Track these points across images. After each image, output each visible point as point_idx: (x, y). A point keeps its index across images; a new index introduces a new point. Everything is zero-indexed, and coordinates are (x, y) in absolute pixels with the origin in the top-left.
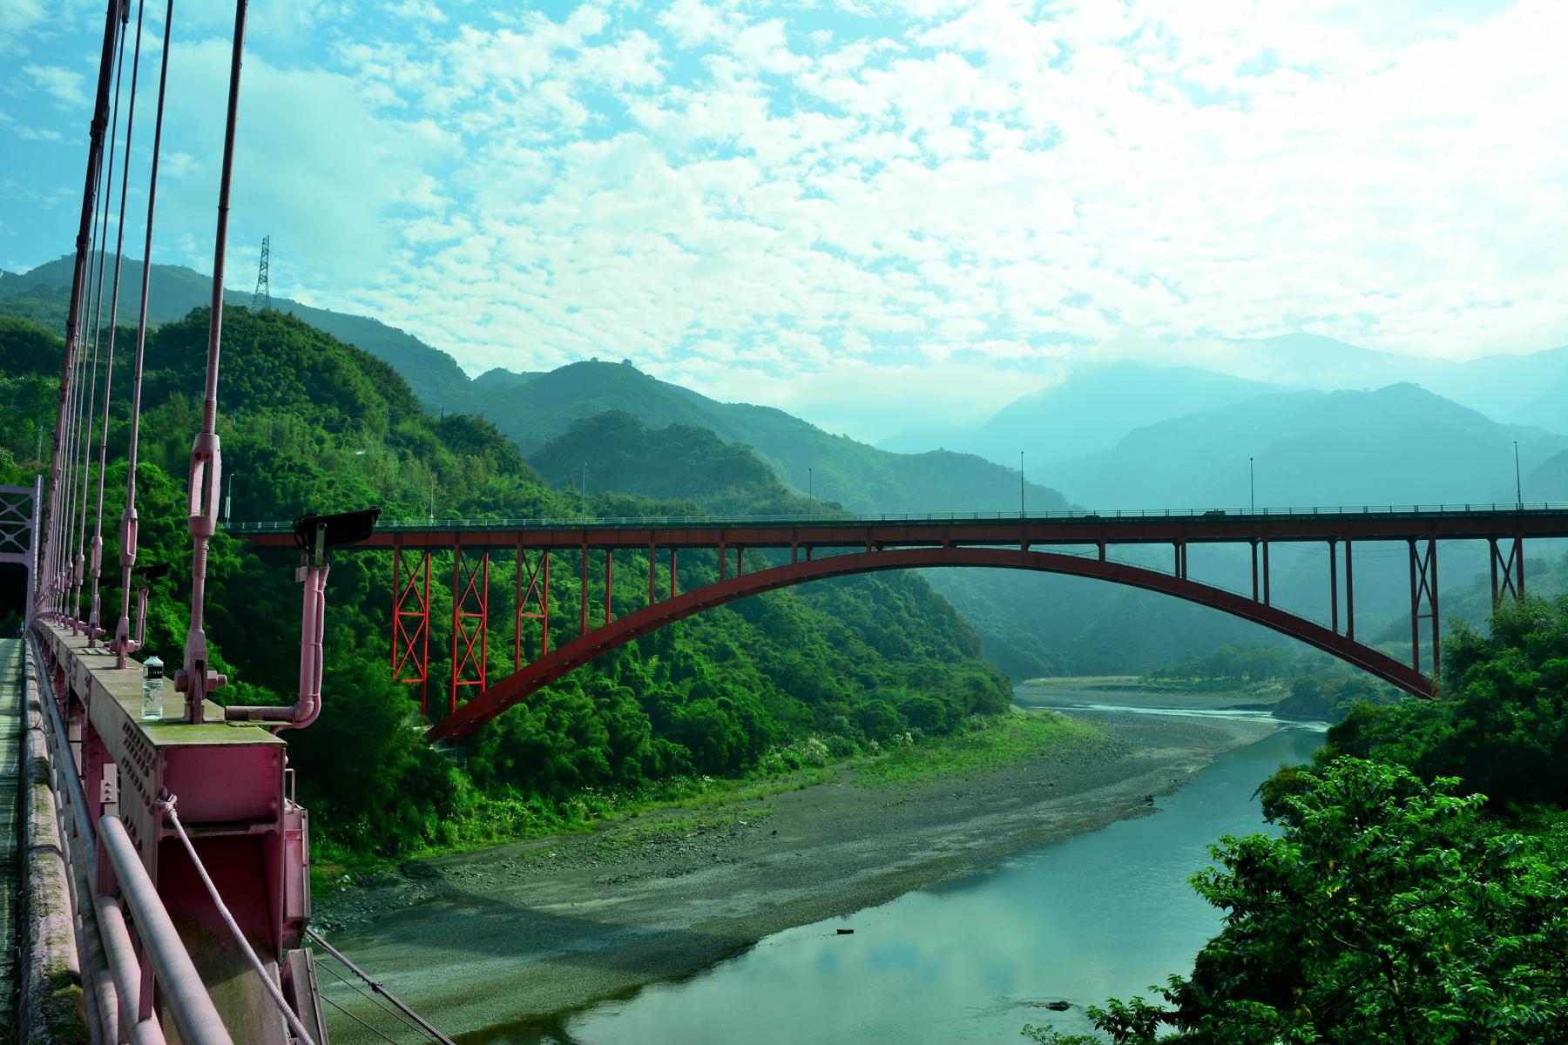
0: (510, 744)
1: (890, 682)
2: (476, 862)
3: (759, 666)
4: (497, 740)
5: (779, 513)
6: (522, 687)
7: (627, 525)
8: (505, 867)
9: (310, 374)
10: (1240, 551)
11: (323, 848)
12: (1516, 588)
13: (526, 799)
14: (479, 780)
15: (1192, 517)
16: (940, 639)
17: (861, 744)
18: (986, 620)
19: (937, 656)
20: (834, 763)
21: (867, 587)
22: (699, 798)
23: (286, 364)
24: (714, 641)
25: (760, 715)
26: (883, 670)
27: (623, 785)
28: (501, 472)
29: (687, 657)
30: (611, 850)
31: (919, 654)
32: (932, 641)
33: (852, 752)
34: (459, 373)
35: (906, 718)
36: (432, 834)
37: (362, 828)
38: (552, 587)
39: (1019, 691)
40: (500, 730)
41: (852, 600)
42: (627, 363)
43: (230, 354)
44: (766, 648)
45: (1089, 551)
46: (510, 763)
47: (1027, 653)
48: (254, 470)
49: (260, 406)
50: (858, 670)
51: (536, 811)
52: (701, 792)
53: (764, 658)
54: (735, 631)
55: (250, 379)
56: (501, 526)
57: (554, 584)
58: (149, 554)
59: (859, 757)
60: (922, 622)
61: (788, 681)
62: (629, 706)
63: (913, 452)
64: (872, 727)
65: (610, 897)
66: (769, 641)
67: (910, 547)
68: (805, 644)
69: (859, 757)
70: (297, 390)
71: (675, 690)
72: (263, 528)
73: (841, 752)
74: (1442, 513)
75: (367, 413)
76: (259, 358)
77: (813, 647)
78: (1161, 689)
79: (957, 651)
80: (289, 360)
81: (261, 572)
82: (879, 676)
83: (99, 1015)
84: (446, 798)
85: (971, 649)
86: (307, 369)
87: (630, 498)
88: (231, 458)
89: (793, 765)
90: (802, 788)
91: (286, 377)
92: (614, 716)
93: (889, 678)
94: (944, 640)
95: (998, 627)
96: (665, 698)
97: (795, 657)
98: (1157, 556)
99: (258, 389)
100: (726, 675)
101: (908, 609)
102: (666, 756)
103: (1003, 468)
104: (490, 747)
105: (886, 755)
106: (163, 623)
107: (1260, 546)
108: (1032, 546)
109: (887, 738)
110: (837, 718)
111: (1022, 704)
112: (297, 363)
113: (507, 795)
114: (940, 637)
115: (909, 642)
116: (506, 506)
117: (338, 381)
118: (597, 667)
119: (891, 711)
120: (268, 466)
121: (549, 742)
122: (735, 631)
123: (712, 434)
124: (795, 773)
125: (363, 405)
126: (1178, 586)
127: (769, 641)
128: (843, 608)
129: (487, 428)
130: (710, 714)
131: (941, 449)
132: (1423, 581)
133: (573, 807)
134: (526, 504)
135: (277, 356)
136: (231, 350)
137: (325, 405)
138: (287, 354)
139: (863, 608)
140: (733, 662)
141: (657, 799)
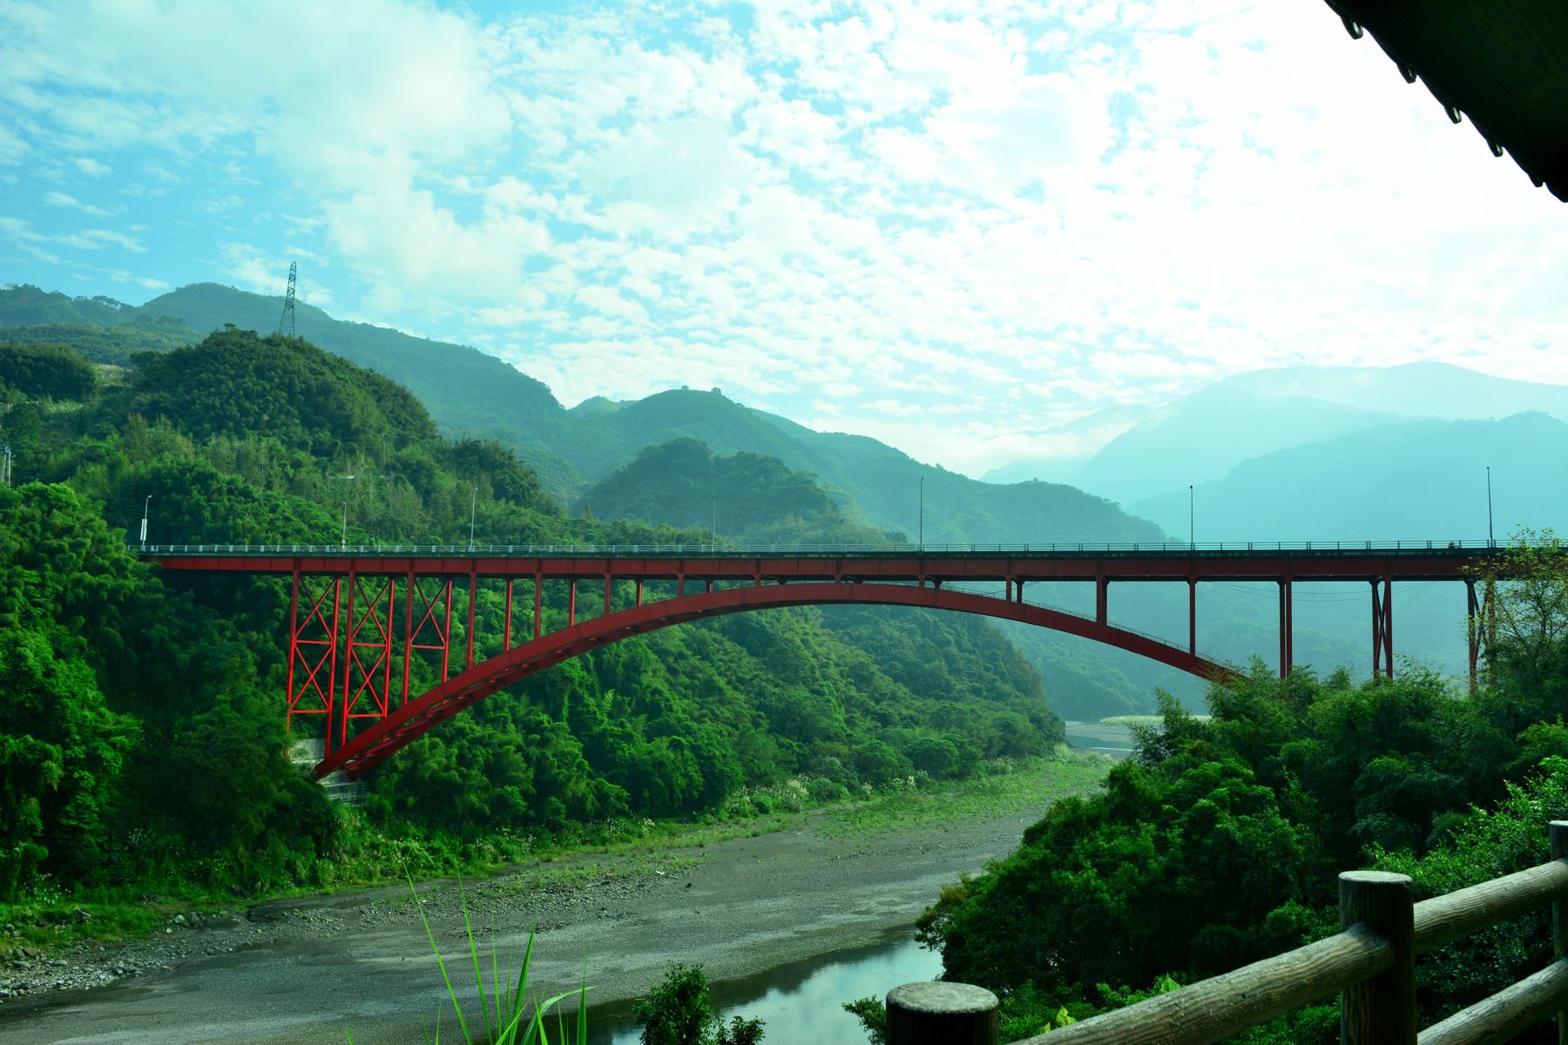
0: (410, 780)
1: (911, 721)
2: (334, 906)
3: (754, 702)
4: (396, 777)
5: (830, 542)
6: (432, 717)
7: (640, 554)
8: (362, 912)
9: (302, 398)
11: (170, 885)
13: (427, 839)
14: (375, 817)
15: (1109, 552)
17: (851, 788)
18: (1071, 655)
19: (984, 693)
20: (814, 807)
21: (915, 620)
22: (636, 841)
23: (278, 387)
24: (700, 675)
25: (724, 756)
26: (908, 708)
27: (514, 826)
28: (497, 497)
29: (656, 691)
30: (493, 898)
31: (962, 691)
32: (981, 677)
33: (839, 797)
34: (552, 401)
35: (910, 762)
36: (304, 873)
37: (219, 867)
38: (514, 616)
40: (401, 765)
42: (716, 391)
43: (224, 377)
44: (764, 684)
45: (995, 589)
46: (411, 801)
47: (1112, 690)
48: (189, 493)
49: (246, 430)
50: (878, 708)
51: (433, 851)
52: (640, 836)
53: (761, 694)
54: (733, 665)
55: (238, 404)
56: (487, 553)
57: (517, 614)
58: (32, 576)
59: (847, 804)
60: (973, 657)
61: (787, 722)
63: (1006, 483)
64: (870, 770)
65: (451, 952)
66: (770, 676)
67: (803, 582)
68: (817, 680)
69: (847, 804)
70: (288, 414)
72: (174, 552)
73: (823, 796)
74: (1399, 550)
75: (362, 436)
76: (249, 382)
77: (824, 683)
79: (1007, 688)
80: (282, 383)
81: (160, 596)
82: (900, 714)
83: (421, 987)
84: (330, 833)
85: (1030, 687)
86: (301, 393)
87: (647, 526)
88: (169, 481)
89: (762, 809)
90: (755, 835)
91: (277, 401)
92: (543, 755)
93: (911, 718)
94: (994, 677)
96: (612, 736)
97: (800, 693)
99: (244, 412)
100: (705, 711)
101: (959, 644)
102: (602, 797)
103: (1098, 500)
104: (389, 782)
105: (878, 800)
106: (22, 646)
107: (1381, 586)
109: (885, 781)
110: (828, 759)
112: (289, 388)
113: (406, 835)
115: (952, 679)
116: (494, 533)
117: (333, 405)
119: (890, 752)
120: (206, 491)
121: (459, 779)
122: (733, 665)
124: (762, 817)
125: (357, 429)
127: (770, 676)
128: (886, 642)
129: (503, 454)
130: (657, 754)
131: (1035, 479)
133: (480, 850)
134: (513, 532)
135: (270, 380)
136: (226, 374)
137: (316, 429)
138: (280, 378)
139: (907, 641)
141: (584, 843)
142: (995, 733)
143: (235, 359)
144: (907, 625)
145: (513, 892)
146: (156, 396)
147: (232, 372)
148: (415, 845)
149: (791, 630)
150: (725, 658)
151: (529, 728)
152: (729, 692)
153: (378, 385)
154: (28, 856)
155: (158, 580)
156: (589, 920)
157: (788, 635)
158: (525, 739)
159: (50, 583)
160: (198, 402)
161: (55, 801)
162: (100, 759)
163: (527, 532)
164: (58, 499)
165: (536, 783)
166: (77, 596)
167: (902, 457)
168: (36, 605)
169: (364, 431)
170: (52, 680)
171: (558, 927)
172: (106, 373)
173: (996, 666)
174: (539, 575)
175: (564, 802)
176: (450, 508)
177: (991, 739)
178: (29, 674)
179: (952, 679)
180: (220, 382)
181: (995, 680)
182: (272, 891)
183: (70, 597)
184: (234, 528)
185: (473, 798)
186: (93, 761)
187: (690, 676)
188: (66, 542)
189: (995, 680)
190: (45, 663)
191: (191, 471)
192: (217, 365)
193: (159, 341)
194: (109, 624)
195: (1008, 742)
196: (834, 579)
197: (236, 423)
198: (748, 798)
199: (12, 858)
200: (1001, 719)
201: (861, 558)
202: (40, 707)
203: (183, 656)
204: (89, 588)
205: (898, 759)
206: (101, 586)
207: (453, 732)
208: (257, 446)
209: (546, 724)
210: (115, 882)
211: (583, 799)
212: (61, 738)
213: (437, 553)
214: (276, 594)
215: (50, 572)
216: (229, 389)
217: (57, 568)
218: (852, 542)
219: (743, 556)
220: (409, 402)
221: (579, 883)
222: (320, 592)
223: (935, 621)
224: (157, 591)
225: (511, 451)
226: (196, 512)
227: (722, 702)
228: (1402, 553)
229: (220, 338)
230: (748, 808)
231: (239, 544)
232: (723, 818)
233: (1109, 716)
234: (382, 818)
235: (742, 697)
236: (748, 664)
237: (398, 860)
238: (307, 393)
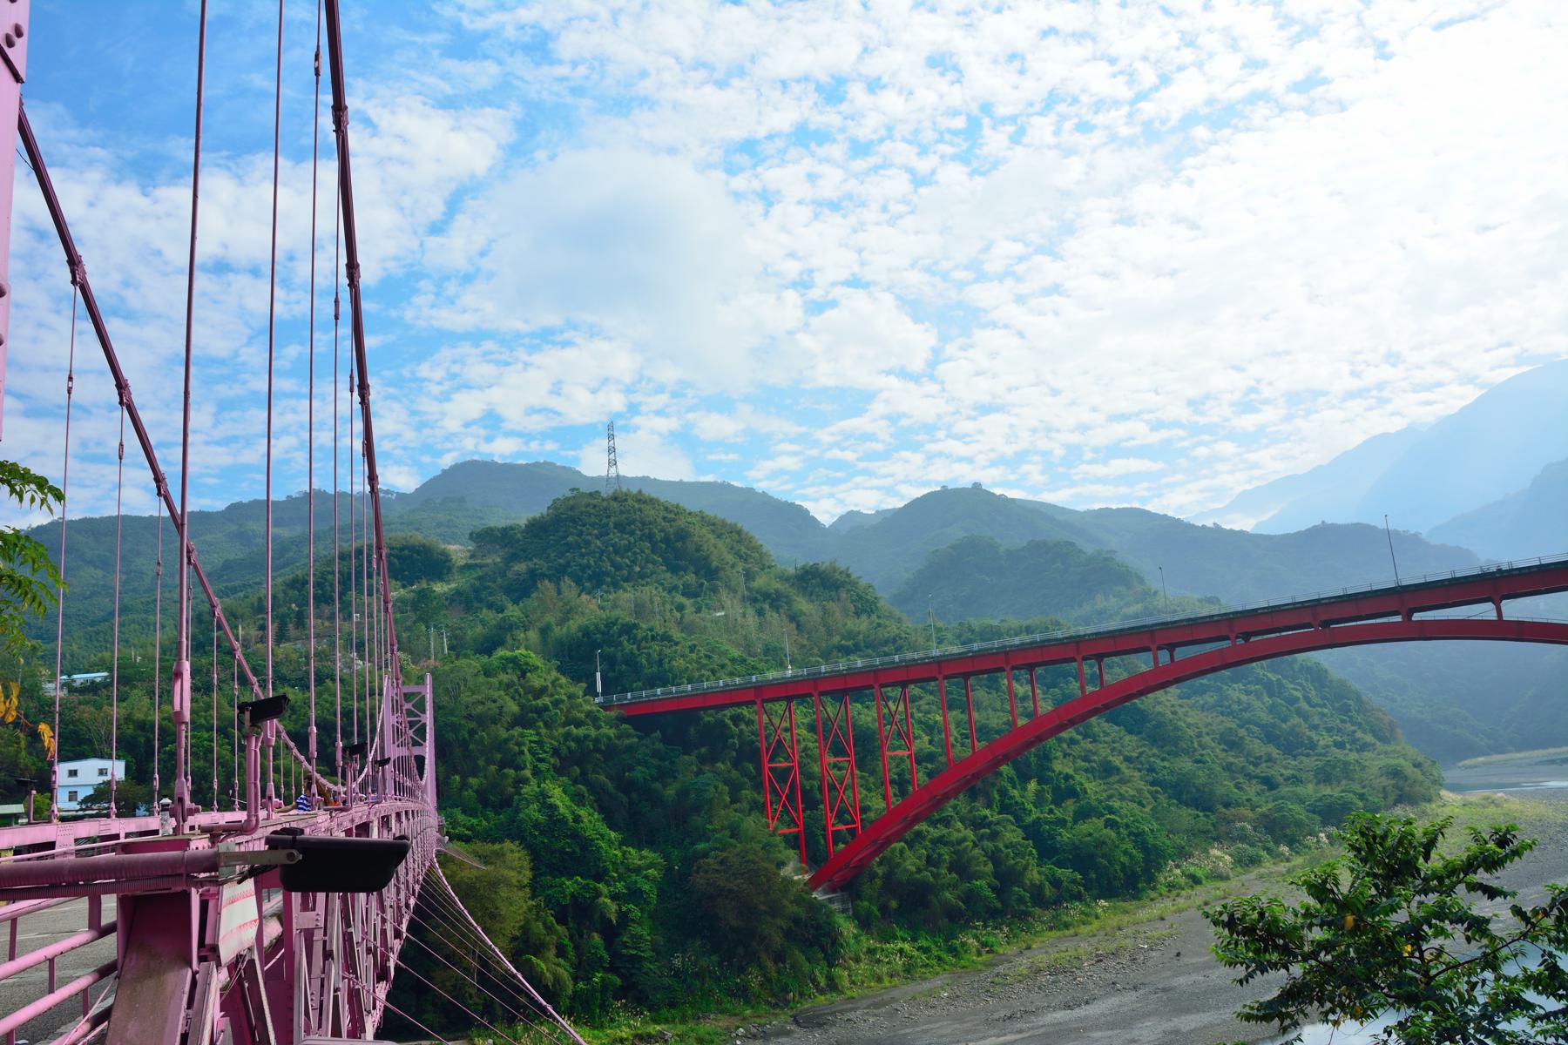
3: (1148, 778)
4: (878, 882)
6: (899, 822)
8: (897, 1010)
9: (664, 546)
13: (914, 940)
14: (864, 923)
17: (1268, 850)
19: (1348, 746)
22: (1096, 924)
23: (640, 539)
24: (1095, 758)
25: (1152, 831)
29: (1067, 777)
30: (1005, 985)
31: (1328, 746)
32: (1339, 730)
33: (1260, 861)
35: (1318, 818)
36: (823, 983)
37: (754, 980)
40: (880, 871)
41: (1244, 698)
43: (589, 537)
44: (1152, 759)
45: (1484, 611)
48: (620, 644)
50: (1258, 771)
51: (925, 950)
52: (1097, 917)
53: (1151, 770)
54: (1117, 745)
55: (610, 560)
60: (1326, 711)
61: (1183, 792)
62: (1013, 835)
65: (1005, 1035)
70: (654, 562)
75: (722, 574)
76: (615, 538)
77: (1204, 752)
79: (1369, 738)
80: (643, 535)
82: (1282, 775)
86: (661, 541)
87: (995, 623)
89: (1195, 880)
91: (643, 552)
92: (996, 847)
93: (1294, 777)
94: (1353, 728)
97: (1186, 764)
99: (618, 567)
102: (1056, 883)
104: (871, 889)
109: (1298, 841)
110: (1238, 825)
112: (650, 537)
113: (895, 937)
114: (1348, 725)
115: (1313, 734)
116: (867, 647)
119: (1299, 811)
120: (633, 640)
121: (931, 879)
122: (1117, 745)
124: (1198, 888)
127: (1155, 751)
128: (1235, 707)
129: (841, 573)
131: (1323, 522)
133: (963, 944)
134: (886, 643)
135: (632, 533)
137: (682, 573)
138: (641, 530)
141: (1051, 929)
142: (1385, 781)
143: (593, 519)
144: (1252, 688)
145: (1020, 978)
146: (531, 565)
147: (596, 532)
148: (906, 946)
149: (1159, 703)
150: (1106, 739)
151: (977, 824)
153: (714, 524)
154: (605, 985)
155: (627, 726)
156: (1108, 995)
157: (1159, 709)
158: (976, 835)
159: (546, 739)
160: (572, 564)
161: (611, 932)
162: (641, 891)
163: (899, 642)
164: (527, 664)
165: (996, 875)
166: (569, 748)
168: (541, 760)
169: (723, 569)
170: (582, 825)
171: (1087, 1003)
172: (458, 551)
173: (1350, 717)
176: (822, 629)
177: (1384, 788)
178: (563, 821)
179: (1313, 734)
180: (588, 543)
181: (1355, 732)
182: (802, 1001)
183: (564, 751)
184: (671, 670)
186: (635, 895)
187: (1085, 759)
188: (546, 700)
189: (1355, 732)
190: (573, 812)
191: (614, 624)
192: (579, 528)
193: (449, 521)
194: (594, 771)
195: (1401, 789)
197: (612, 578)
198: (1178, 871)
199: (593, 986)
200: (1387, 766)
201: (1329, 603)
202: (578, 850)
203: (671, 792)
204: (577, 740)
205: (1307, 817)
206: (586, 737)
207: (912, 836)
208: (649, 593)
209: (991, 819)
210: (672, 1005)
211: (1040, 887)
212: (600, 876)
213: (901, 661)
214: (726, 726)
215: (543, 731)
216: (599, 547)
217: (547, 725)
218: (1175, 611)
219: (1216, 618)
220: (743, 536)
224: (628, 736)
226: (631, 661)
227: (1123, 781)
229: (571, 502)
230: (1182, 880)
231: (679, 685)
232: (1163, 892)
233: (1465, 759)
234: (869, 924)
235: (1137, 774)
236: (1131, 743)
237: (899, 962)
238: (666, 540)
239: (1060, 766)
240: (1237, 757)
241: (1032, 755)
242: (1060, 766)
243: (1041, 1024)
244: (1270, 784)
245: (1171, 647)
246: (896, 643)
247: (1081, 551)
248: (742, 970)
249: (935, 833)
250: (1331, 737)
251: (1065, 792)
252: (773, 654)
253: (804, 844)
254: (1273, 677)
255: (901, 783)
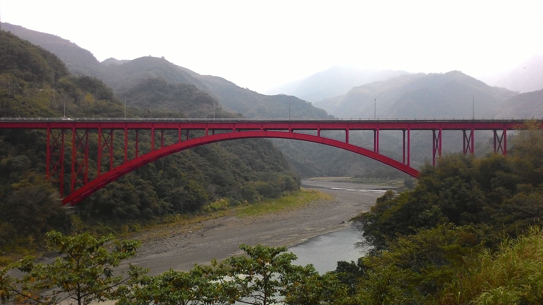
10: (398, 134)
12: (471, 148)
14: (84, 218)
16: (276, 163)
29: (175, 170)
31: (268, 169)
34: (94, 59)
39: (303, 182)
40: (93, 198)
41: (244, 149)
45: (314, 133)
53: (206, 170)
61: (218, 181)
62: (151, 189)
67: (274, 131)
71: (169, 183)
78: (358, 182)
79: (282, 168)
82: (251, 176)
95: (301, 159)
98: (338, 135)
102: (164, 207)
105: (250, 206)
107: (406, 132)
108: (294, 131)
111: (305, 186)
114: (276, 162)
118: (138, 174)
123: (194, 86)
126: (346, 146)
132: (468, 145)
137: (25, 70)
140: (193, 171)
152: (197, 170)
167: (233, 85)
171: (165, 252)
174: (126, 129)
175: (152, 209)
185: (120, 209)
189: (278, 165)
196: (260, 130)
221: (165, 237)
222: (82, 135)
223: (257, 145)
225: (102, 80)
227: (195, 173)
228: (370, 122)
239: (174, 166)
240: (237, 169)
241: (162, 160)
242: (174, 166)
243: (146, 259)
244: (247, 179)
245: (214, 130)
246: (119, 113)
247: (197, 89)
248: (26, 235)
249: (119, 186)
250: (270, 166)
251: (173, 175)
252: (61, 111)
253: (61, 187)
254: (255, 143)
255: (108, 166)
